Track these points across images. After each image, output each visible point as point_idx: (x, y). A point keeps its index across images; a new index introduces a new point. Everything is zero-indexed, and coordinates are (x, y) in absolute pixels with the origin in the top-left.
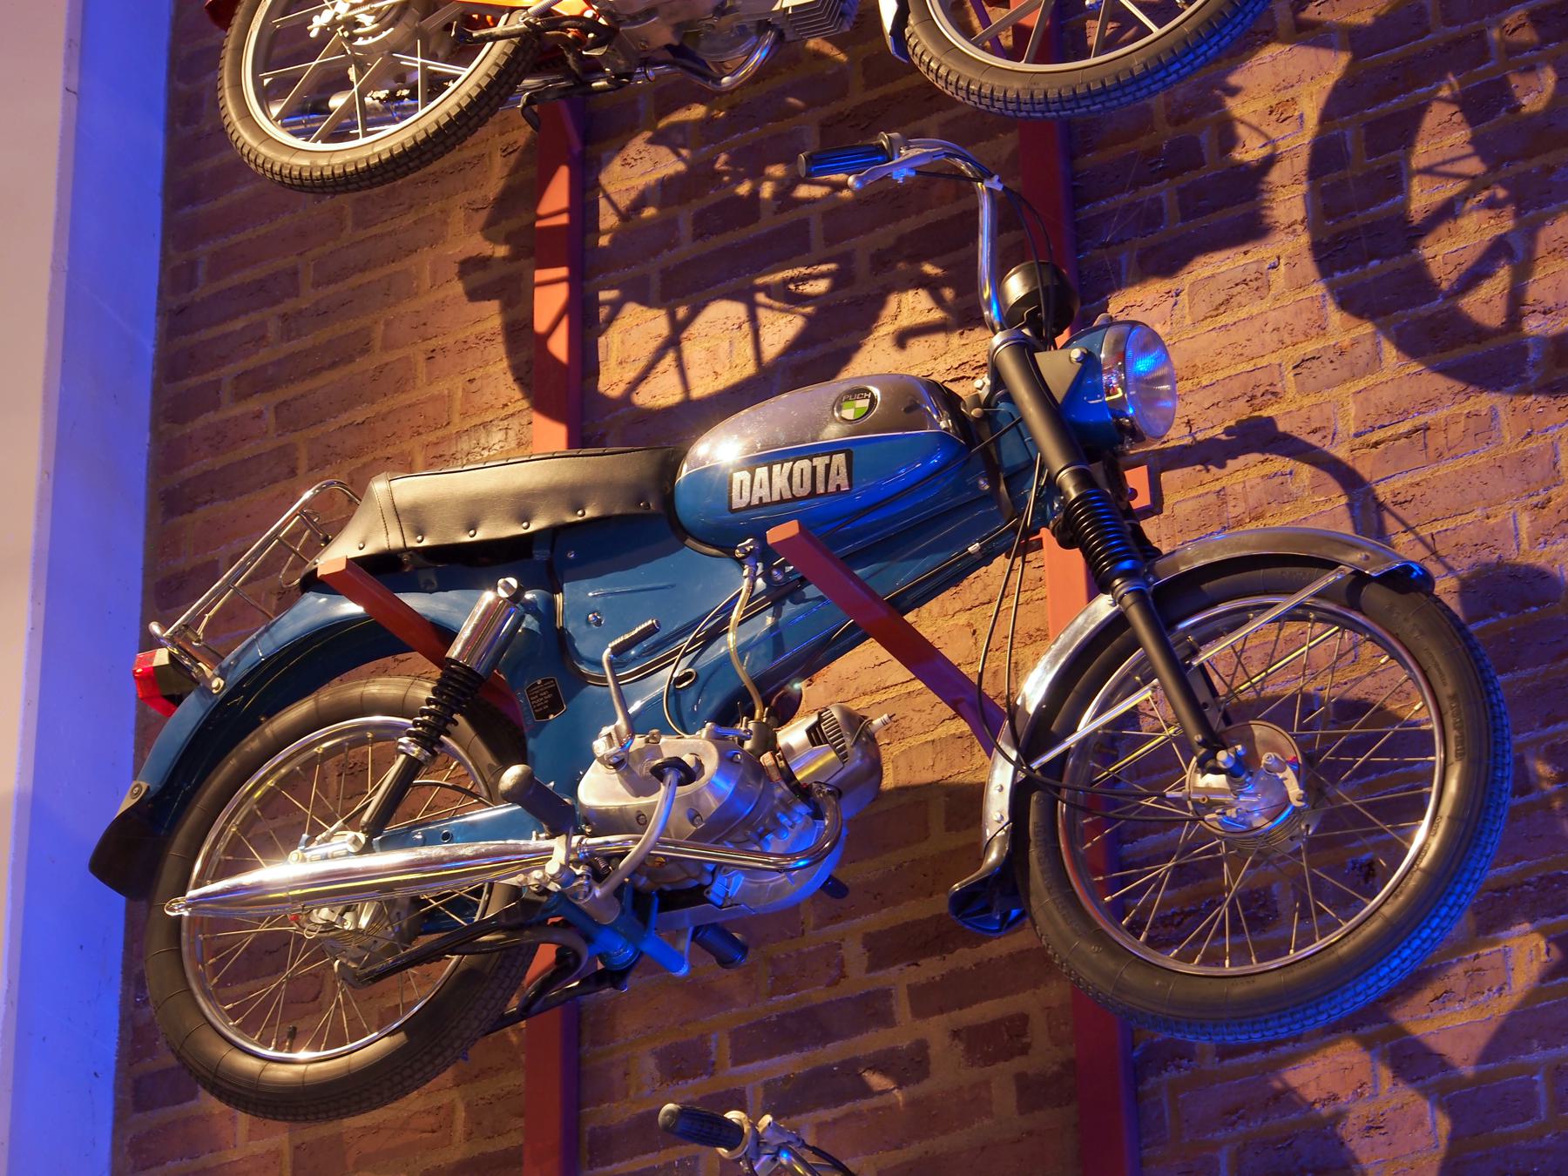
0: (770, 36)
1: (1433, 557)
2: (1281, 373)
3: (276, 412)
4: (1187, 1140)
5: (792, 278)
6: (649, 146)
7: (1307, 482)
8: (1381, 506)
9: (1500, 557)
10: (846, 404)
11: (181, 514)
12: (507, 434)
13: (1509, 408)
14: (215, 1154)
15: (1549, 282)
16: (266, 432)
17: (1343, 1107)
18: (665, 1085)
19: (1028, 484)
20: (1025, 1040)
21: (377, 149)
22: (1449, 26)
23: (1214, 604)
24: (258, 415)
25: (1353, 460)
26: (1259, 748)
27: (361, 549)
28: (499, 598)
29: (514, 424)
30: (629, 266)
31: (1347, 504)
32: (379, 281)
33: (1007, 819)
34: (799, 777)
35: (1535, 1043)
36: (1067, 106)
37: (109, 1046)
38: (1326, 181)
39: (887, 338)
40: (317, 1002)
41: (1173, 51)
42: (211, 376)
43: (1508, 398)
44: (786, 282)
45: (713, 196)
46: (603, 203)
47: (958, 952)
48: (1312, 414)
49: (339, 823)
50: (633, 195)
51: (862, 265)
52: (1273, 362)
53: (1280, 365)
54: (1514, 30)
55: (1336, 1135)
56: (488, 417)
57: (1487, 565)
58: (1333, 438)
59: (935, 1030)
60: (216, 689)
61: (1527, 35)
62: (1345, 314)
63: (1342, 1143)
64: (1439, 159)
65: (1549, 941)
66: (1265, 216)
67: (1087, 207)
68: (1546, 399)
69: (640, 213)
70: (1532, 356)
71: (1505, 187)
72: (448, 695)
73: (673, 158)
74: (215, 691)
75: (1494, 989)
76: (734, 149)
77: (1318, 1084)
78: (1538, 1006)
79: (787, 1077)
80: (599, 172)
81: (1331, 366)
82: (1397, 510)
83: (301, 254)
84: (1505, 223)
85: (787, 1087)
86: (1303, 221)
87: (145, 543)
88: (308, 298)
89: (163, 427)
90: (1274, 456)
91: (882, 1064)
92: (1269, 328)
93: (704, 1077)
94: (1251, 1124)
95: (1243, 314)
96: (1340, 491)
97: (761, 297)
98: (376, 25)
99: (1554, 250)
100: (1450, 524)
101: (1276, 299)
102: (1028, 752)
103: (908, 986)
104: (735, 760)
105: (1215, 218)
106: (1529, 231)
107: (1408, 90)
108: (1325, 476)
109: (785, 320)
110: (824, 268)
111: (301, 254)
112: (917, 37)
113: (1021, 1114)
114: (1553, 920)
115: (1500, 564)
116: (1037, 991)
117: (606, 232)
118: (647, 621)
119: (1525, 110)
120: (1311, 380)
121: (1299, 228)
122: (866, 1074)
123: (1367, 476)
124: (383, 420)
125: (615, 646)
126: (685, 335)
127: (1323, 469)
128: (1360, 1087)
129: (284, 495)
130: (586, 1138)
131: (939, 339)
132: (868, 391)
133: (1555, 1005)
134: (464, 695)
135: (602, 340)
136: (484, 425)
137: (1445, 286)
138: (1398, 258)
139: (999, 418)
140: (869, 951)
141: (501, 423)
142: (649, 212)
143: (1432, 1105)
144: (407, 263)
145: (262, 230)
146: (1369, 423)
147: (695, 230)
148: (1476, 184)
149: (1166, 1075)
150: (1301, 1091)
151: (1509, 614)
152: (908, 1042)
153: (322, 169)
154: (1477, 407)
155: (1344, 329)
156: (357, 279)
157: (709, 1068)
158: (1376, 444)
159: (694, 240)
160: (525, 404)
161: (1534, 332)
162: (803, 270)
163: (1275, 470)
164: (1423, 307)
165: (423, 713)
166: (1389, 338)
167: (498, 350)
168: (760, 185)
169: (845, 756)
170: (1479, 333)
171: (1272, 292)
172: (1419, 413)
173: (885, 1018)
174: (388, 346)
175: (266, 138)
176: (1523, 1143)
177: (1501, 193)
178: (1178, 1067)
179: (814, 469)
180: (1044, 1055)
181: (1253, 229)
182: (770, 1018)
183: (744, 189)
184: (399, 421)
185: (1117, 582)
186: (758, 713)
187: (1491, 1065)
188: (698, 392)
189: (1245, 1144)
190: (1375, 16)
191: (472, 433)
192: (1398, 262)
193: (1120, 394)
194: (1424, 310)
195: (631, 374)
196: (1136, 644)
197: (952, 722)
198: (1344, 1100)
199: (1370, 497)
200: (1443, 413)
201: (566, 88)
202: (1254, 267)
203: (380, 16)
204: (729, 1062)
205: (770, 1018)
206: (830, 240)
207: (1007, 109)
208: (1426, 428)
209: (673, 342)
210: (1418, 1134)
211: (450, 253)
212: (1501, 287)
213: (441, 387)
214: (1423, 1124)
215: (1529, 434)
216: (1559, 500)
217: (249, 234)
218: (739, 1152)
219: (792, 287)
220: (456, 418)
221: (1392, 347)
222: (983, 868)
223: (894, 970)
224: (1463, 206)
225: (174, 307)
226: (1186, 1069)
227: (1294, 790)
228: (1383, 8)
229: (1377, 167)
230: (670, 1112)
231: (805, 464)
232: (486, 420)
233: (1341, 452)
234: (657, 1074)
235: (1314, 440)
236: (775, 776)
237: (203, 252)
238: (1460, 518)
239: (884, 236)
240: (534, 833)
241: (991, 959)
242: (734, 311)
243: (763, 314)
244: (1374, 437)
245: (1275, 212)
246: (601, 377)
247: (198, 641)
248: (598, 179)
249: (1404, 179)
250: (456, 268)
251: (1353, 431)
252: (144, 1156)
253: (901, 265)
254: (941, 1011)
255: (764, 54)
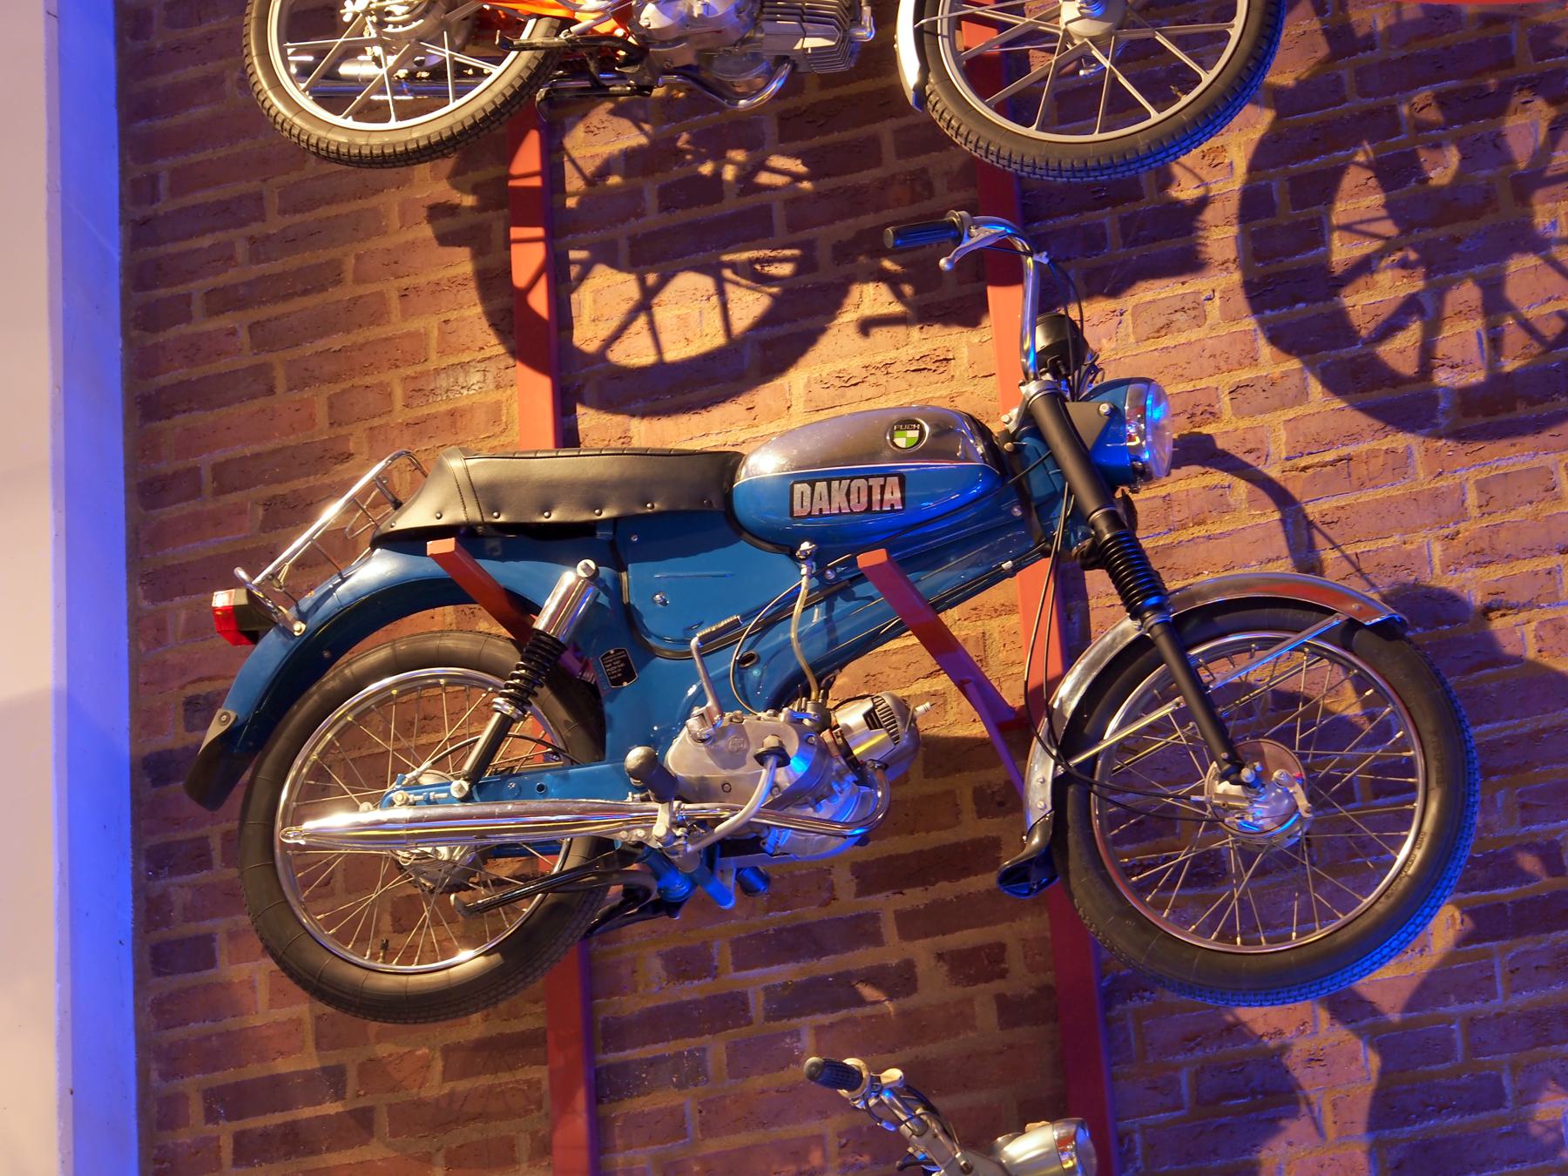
0: (785, 71)
1: (1357, 573)
2: (1218, 396)
3: (250, 332)
4: (1151, 1061)
5: (758, 259)
6: (611, 117)
7: (1244, 497)
8: (1310, 524)
9: (1416, 579)
10: (897, 433)
11: (160, 420)
12: (485, 375)
13: (1423, 448)
14: (237, 1018)
15: (1456, 340)
16: (241, 350)
17: (1288, 1041)
18: (671, 984)
19: (1056, 511)
20: (1003, 966)
21: (415, 135)
22: (1363, 97)
23: (1224, 635)
24: (232, 333)
25: (1285, 481)
26: (1270, 764)
27: (439, 518)
28: (579, 578)
29: (492, 367)
30: (598, 230)
31: (1281, 520)
32: (347, 215)
33: (1049, 808)
34: (856, 752)
35: (1452, 998)
36: (1078, 174)
37: (127, 917)
38: (1255, 226)
39: (851, 324)
40: (328, 887)
41: (1173, 137)
42: (180, 289)
43: (1421, 439)
44: (752, 262)
45: (677, 172)
46: (568, 167)
47: (937, 886)
48: (1247, 436)
49: (427, 764)
50: (598, 162)
51: (824, 254)
52: (1211, 385)
53: (1217, 389)
54: (1422, 109)
55: (1282, 1064)
56: (465, 358)
57: (1405, 584)
58: (1266, 460)
59: (921, 951)
60: (299, 631)
61: (1433, 115)
62: (1275, 349)
63: (1287, 1072)
64: (1357, 218)
65: (1463, 912)
66: (1200, 252)
67: (1036, 225)
68: (1455, 444)
69: (605, 180)
70: (1442, 404)
71: (1416, 250)
72: (536, 662)
73: (635, 131)
74: (296, 634)
75: (1417, 950)
76: (694, 131)
77: (1265, 1020)
78: (1454, 967)
79: (786, 983)
80: (563, 136)
81: (1265, 394)
82: (1325, 528)
83: (265, 180)
84: (1414, 284)
85: (786, 993)
86: (1235, 260)
87: (124, 443)
88: (275, 224)
89: (135, 333)
90: (1213, 470)
91: (875, 977)
92: (1207, 354)
93: (709, 979)
94: (1208, 1050)
95: (1182, 338)
96: (1273, 507)
97: (728, 273)
98: (406, 16)
99: (1460, 312)
100: (1372, 546)
101: (1212, 329)
102: (1065, 752)
103: (895, 912)
104: (809, 741)
105: (1154, 248)
106: (1439, 293)
107: (1327, 151)
108: (1260, 493)
109: (751, 297)
110: (788, 252)
111: (265, 180)
112: (937, 95)
113: (1001, 1029)
114: (1466, 896)
115: (1415, 585)
116: (1013, 924)
117: (573, 195)
118: (732, 615)
119: (1433, 183)
120: (1245, 405)
121: (1232, 266)
122: (859, 986)
123: (1297, 496)
124: (360, 350)
125: (703, 636)
126: (656, 301)
127: (1259, 486)
128: (1303, 1025)
129: (263, 411)
130: (600, 1026)
131: (900, 331)
132: (917, 423)
133: (1469, 967)
134: (549, 661)
135: (574, 297)
136: (462, 365)
137: (1364, 333)
138: (1321, 303)
139: (1027, 453)
140: (857, 878)
141: (478, 365)
142: (614, 180)
143: (1365, 1044)
144: (374, 201)
145: (222, 152)
146: (1298, 450)
147: (660, 203)
148: (1390, 246)
149: (1130, 1004)
150: (1251, 1025)
151: (1425, 629)
152: (897, 961)
153: (360, 147)
154: (1394, 445)
155: (1272, 363)
156: (323, 212)
157: (711, 971)
158: (1304, 469)
159: (660, 212)
160: (500, 350)
161: (1443, 384)
162: (769, 253)
163: (1216, 483)
164: (1345, 350)
165: (514, 677)
166: (1315, 375)
167: (471, 294)
168: (722, 167)
169: (897, 738)
170: (1394, 379)
171: (1208, 322)
172: (1343, 445)
173: (876, 939)
174: (359, 280)
175: (299, 110)
176: (1443, 1080)
177: (1413, 256)
178: (1142, 998)
179: (870, 488)
180: (1020, 979)
181: (1189, 262)
182: (767, 931)
183: (706, 169)
184: (376, 353)
185: (1147, 615)
186: (813, 695)
187: (1415, 1014)
188: (671, 355)
189: (1202, 1068)
190: (1296, 79)
191: (450, 372)
192: (1321, 307)
193: (1138, 441)
194: (1346, 353)
195: (605, 330)
196: (1160, 661)
197: (926, 680)
198: (1288, 1035)
199: (1300, 515)
200: (1364, 447)
201: (583, 89)
202: (1190, 299)
203: (412, 7)
204: (731, 968)
205: (767, 931)
206: (793, 226)
207: (1022, 171)
208: (1349, 459)
209: (644, 306)
210: (1353, 1068)
211: (418, 196)
212: (1413, 340)
213: (416, 325)
214: (1357, 1060)
215: (1440, 474)
216: (1467, 534)
217: (207, 154)
218: (858, 1093)
219: (758, 267)
220: (434, 356)
221: (1318, 383)
222: (1027, 850)
223: (881, 897)
224: (1379, 263)
225: (137, 218)
226: (1148, 1000)
227: (1303, 803)
228: (1303, 73)
229: (1302, 219)
230: (813, 1064)
231: (861, 483)
232: (463, 360)
233: (1274, 472)
234: (664, 974)
235: (1248, 459)
236: (834, 751)
237: (164, 166)
238: (1380, 541)
239: (844, 229)
240: (630, 794)
241: (970, 893)
242: (706, 283)
243: (729, 288)
244: (1303, 462)
245: (1209, 250)
246: (575, 331)
247: (280, 588)
248: (562, 143)
249: (1326, 232)
250: (424, 213)
251: (1284, 455)
252: (167, 1016)
253: (862, 259)
254: (926, 936)
255: (780, 84)
